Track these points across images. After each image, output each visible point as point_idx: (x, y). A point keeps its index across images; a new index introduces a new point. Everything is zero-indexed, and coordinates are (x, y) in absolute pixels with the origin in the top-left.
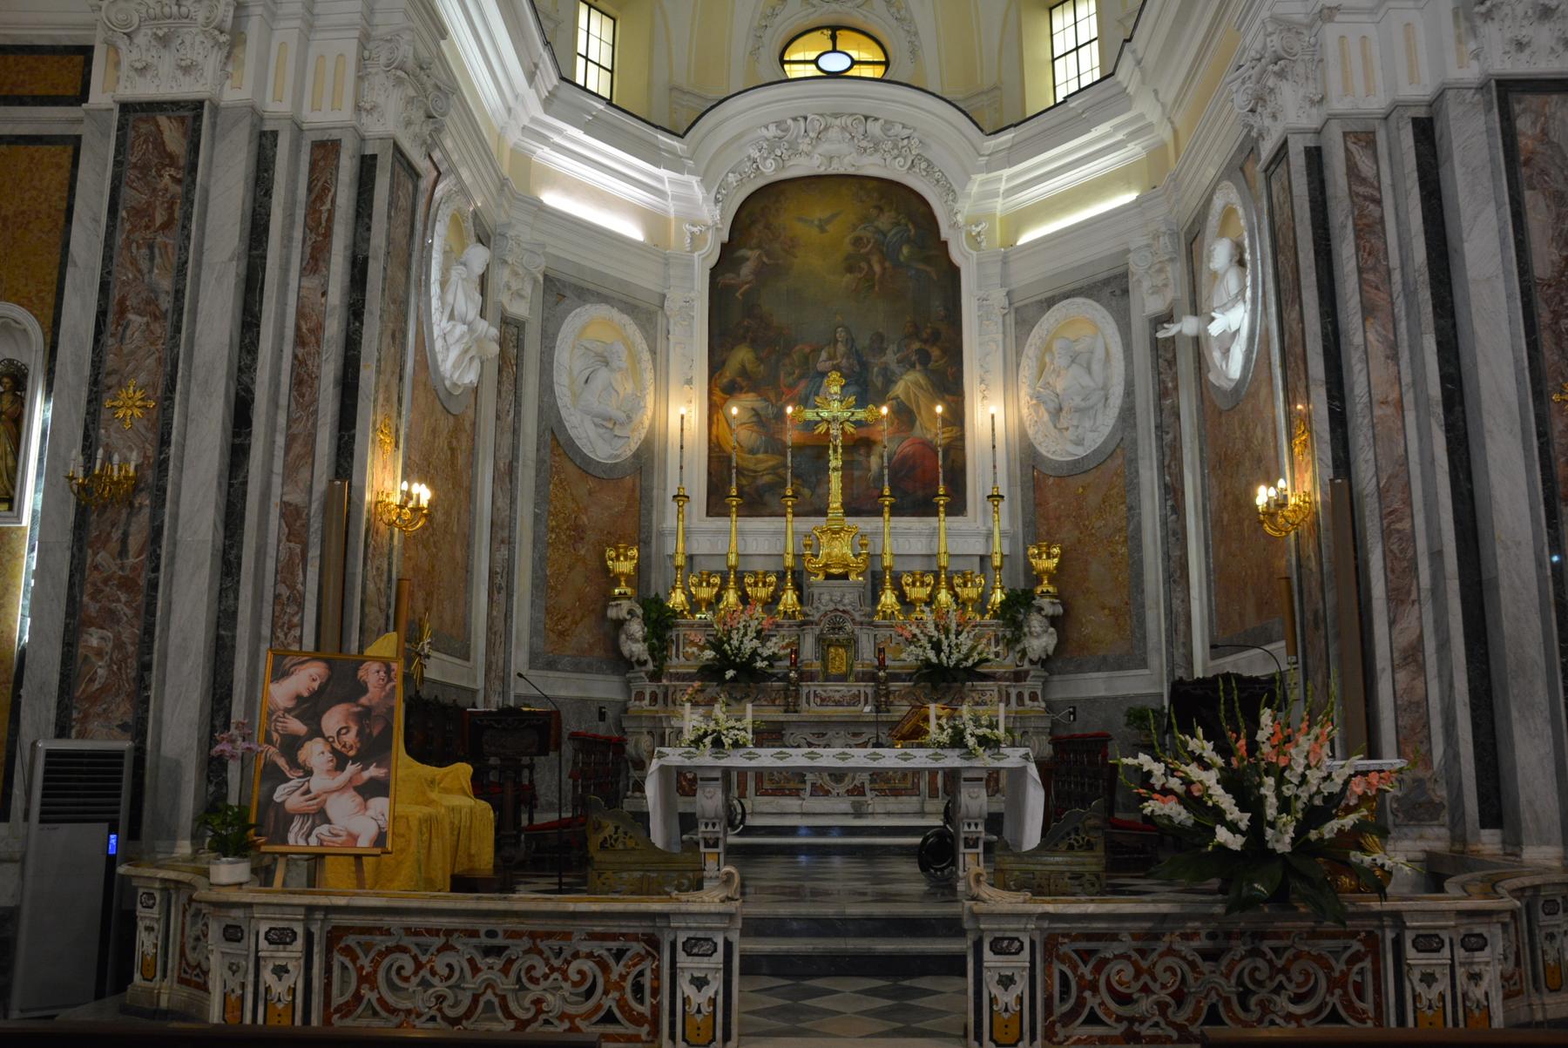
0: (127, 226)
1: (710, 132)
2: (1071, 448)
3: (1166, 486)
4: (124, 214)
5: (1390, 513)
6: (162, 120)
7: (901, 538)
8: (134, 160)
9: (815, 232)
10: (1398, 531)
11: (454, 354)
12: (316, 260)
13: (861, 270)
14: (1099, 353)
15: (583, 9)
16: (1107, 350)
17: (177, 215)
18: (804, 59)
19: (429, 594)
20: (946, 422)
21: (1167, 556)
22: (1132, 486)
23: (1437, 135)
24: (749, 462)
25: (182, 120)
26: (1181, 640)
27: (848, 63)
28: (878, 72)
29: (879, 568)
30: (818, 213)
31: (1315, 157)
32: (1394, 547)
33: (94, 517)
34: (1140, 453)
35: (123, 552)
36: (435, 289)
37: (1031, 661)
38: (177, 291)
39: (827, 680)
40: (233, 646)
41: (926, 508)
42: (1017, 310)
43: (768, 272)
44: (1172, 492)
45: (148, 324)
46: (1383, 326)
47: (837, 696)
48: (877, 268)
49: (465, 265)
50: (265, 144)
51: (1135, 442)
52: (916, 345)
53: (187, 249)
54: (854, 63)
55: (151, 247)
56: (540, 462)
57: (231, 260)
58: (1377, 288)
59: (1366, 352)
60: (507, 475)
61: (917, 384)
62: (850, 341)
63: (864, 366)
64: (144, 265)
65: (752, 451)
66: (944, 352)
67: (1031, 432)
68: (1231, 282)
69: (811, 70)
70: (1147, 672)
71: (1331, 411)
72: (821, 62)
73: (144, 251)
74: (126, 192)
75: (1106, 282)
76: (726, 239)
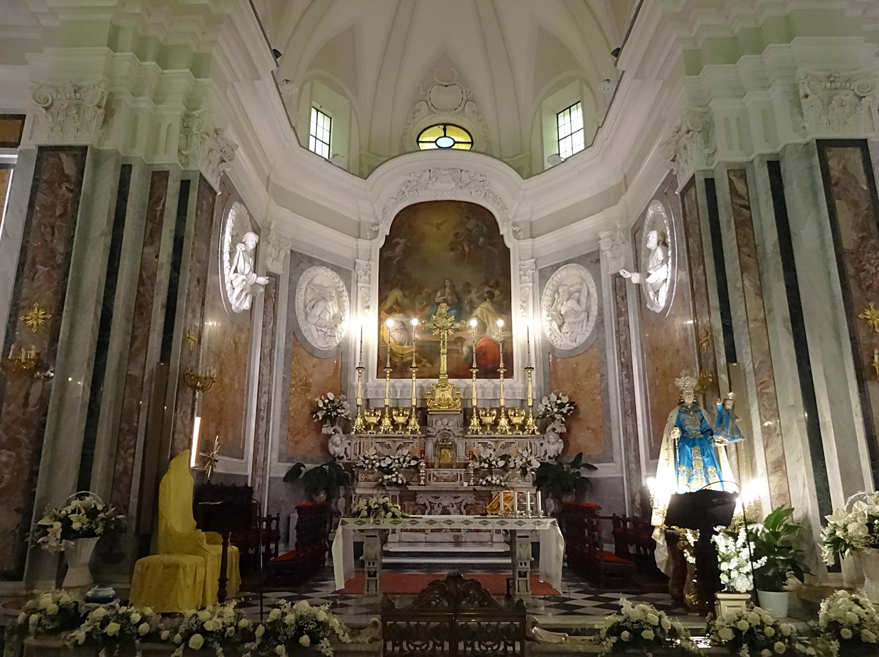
0: (39, 215)
1: (350, 132)
2: (570, 344)
3: (622, 363)
4: (38, 208)
5: (761, 383)
6: (63, 156)
7: (477, 388)
8: (45, 178)
9: (434, 230)
10: (767, 394)
11: (237, 291)
12: (152, 235)
13: (458, 249)
14: (584, 293)
15: (314, 111)
16: (589, 293)
17: (69, 209)
18: (430, 139)
19: (219, 424)
20: (503, 329)
21: (623, 402)
22: (603, 363)
23: (782, 170)
24: (397, 349)
25: (75, 156)
26: (633, 448)
27: (452, 142)
28: (468, 147)
29: (470, 406)
30: (437, 220)
31: (710, 184)
32: (765, 403)
33: (9, 383)
34: (607, 346)
35: (26, 404)
36: (226, 257)
37: (549, 457)
38: (67, 253)
39: (439, 467)
40: (92, 460)
41: (489, 371)
42: (540, 270)
43: (409, 251)
44: (626, 367)
45: (48, 271)
46: (753, 277)
47: (445, 477)
48: (467, 249)
49: (244, 243)
50: (125, 171)
51: (604, 340)
52: (487, 289)
53: (74, 229)
54: (455, 142)
55: (53, 228)
56: (287, 351)
57: (101, 235)
58: (749, 256)
59: (744, 291)
60: (268, 357)
61: (487, 309)
62: (453, 287)
63: (460, 300)
64: (48, 238)
65: (401, 344)
66: (502, 292)
67: (548, 334)
68: (659, 254)
69: (433, 146)
70: (613, 464)
71: (723, 325)
72: (438, 142)
73: (49, 229)
74: (40, 195)
75: (588, 255)
76: (388, 234)
